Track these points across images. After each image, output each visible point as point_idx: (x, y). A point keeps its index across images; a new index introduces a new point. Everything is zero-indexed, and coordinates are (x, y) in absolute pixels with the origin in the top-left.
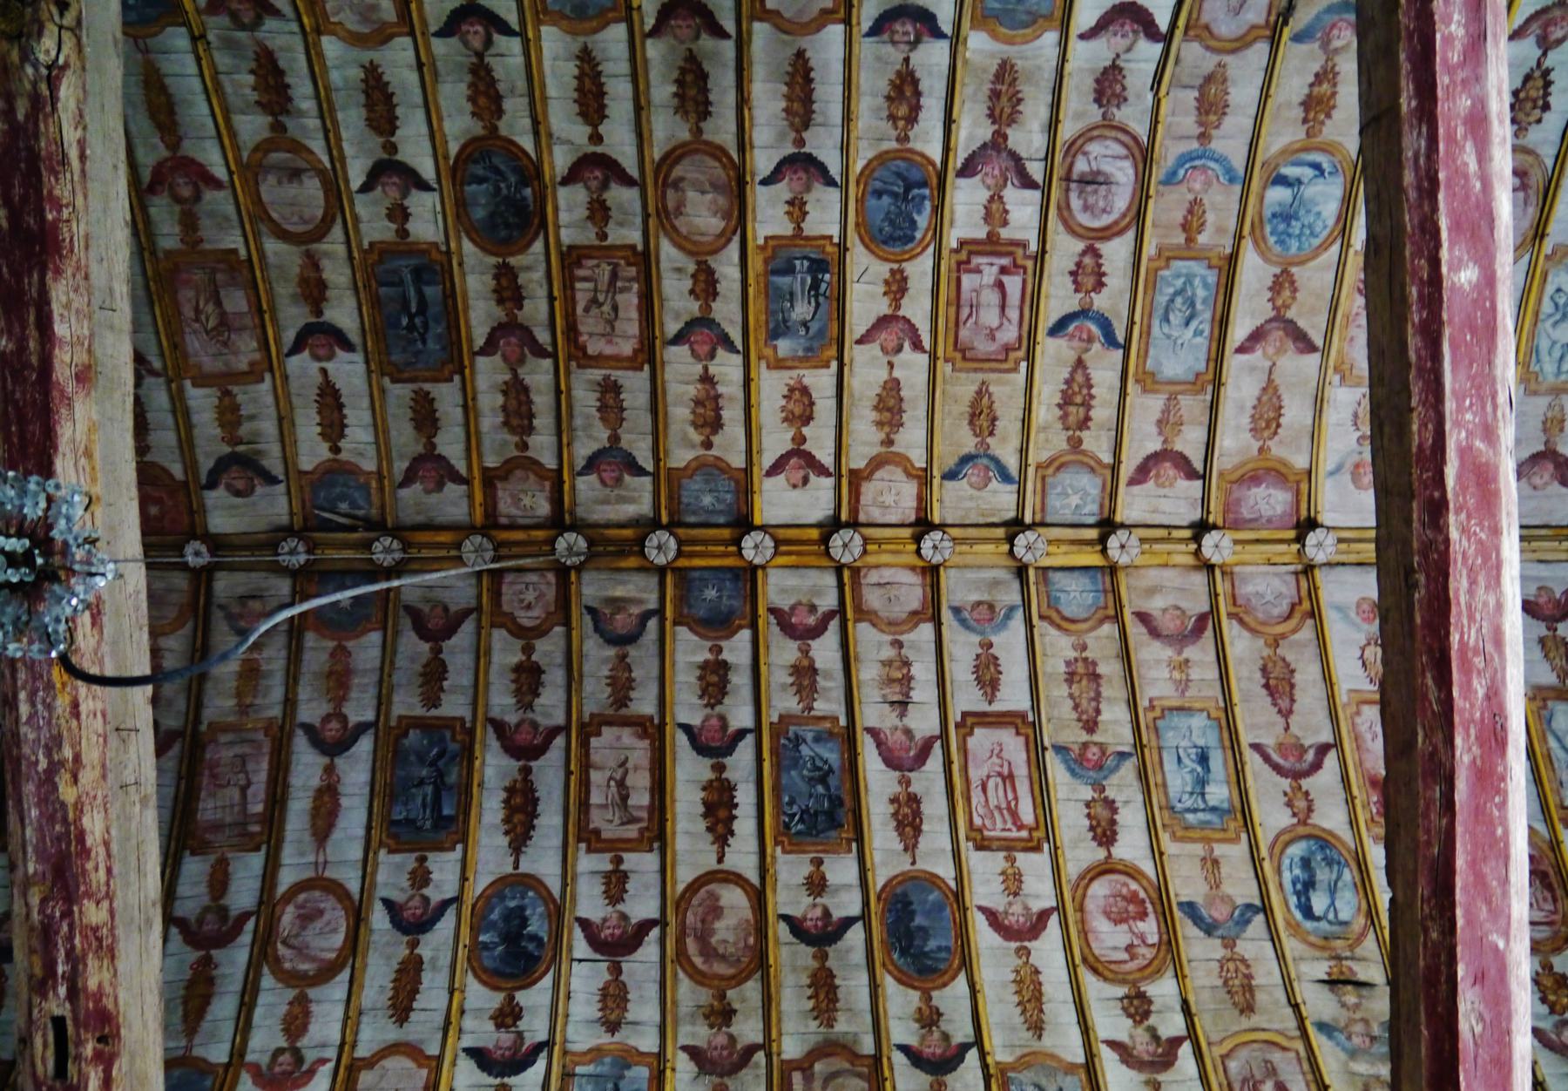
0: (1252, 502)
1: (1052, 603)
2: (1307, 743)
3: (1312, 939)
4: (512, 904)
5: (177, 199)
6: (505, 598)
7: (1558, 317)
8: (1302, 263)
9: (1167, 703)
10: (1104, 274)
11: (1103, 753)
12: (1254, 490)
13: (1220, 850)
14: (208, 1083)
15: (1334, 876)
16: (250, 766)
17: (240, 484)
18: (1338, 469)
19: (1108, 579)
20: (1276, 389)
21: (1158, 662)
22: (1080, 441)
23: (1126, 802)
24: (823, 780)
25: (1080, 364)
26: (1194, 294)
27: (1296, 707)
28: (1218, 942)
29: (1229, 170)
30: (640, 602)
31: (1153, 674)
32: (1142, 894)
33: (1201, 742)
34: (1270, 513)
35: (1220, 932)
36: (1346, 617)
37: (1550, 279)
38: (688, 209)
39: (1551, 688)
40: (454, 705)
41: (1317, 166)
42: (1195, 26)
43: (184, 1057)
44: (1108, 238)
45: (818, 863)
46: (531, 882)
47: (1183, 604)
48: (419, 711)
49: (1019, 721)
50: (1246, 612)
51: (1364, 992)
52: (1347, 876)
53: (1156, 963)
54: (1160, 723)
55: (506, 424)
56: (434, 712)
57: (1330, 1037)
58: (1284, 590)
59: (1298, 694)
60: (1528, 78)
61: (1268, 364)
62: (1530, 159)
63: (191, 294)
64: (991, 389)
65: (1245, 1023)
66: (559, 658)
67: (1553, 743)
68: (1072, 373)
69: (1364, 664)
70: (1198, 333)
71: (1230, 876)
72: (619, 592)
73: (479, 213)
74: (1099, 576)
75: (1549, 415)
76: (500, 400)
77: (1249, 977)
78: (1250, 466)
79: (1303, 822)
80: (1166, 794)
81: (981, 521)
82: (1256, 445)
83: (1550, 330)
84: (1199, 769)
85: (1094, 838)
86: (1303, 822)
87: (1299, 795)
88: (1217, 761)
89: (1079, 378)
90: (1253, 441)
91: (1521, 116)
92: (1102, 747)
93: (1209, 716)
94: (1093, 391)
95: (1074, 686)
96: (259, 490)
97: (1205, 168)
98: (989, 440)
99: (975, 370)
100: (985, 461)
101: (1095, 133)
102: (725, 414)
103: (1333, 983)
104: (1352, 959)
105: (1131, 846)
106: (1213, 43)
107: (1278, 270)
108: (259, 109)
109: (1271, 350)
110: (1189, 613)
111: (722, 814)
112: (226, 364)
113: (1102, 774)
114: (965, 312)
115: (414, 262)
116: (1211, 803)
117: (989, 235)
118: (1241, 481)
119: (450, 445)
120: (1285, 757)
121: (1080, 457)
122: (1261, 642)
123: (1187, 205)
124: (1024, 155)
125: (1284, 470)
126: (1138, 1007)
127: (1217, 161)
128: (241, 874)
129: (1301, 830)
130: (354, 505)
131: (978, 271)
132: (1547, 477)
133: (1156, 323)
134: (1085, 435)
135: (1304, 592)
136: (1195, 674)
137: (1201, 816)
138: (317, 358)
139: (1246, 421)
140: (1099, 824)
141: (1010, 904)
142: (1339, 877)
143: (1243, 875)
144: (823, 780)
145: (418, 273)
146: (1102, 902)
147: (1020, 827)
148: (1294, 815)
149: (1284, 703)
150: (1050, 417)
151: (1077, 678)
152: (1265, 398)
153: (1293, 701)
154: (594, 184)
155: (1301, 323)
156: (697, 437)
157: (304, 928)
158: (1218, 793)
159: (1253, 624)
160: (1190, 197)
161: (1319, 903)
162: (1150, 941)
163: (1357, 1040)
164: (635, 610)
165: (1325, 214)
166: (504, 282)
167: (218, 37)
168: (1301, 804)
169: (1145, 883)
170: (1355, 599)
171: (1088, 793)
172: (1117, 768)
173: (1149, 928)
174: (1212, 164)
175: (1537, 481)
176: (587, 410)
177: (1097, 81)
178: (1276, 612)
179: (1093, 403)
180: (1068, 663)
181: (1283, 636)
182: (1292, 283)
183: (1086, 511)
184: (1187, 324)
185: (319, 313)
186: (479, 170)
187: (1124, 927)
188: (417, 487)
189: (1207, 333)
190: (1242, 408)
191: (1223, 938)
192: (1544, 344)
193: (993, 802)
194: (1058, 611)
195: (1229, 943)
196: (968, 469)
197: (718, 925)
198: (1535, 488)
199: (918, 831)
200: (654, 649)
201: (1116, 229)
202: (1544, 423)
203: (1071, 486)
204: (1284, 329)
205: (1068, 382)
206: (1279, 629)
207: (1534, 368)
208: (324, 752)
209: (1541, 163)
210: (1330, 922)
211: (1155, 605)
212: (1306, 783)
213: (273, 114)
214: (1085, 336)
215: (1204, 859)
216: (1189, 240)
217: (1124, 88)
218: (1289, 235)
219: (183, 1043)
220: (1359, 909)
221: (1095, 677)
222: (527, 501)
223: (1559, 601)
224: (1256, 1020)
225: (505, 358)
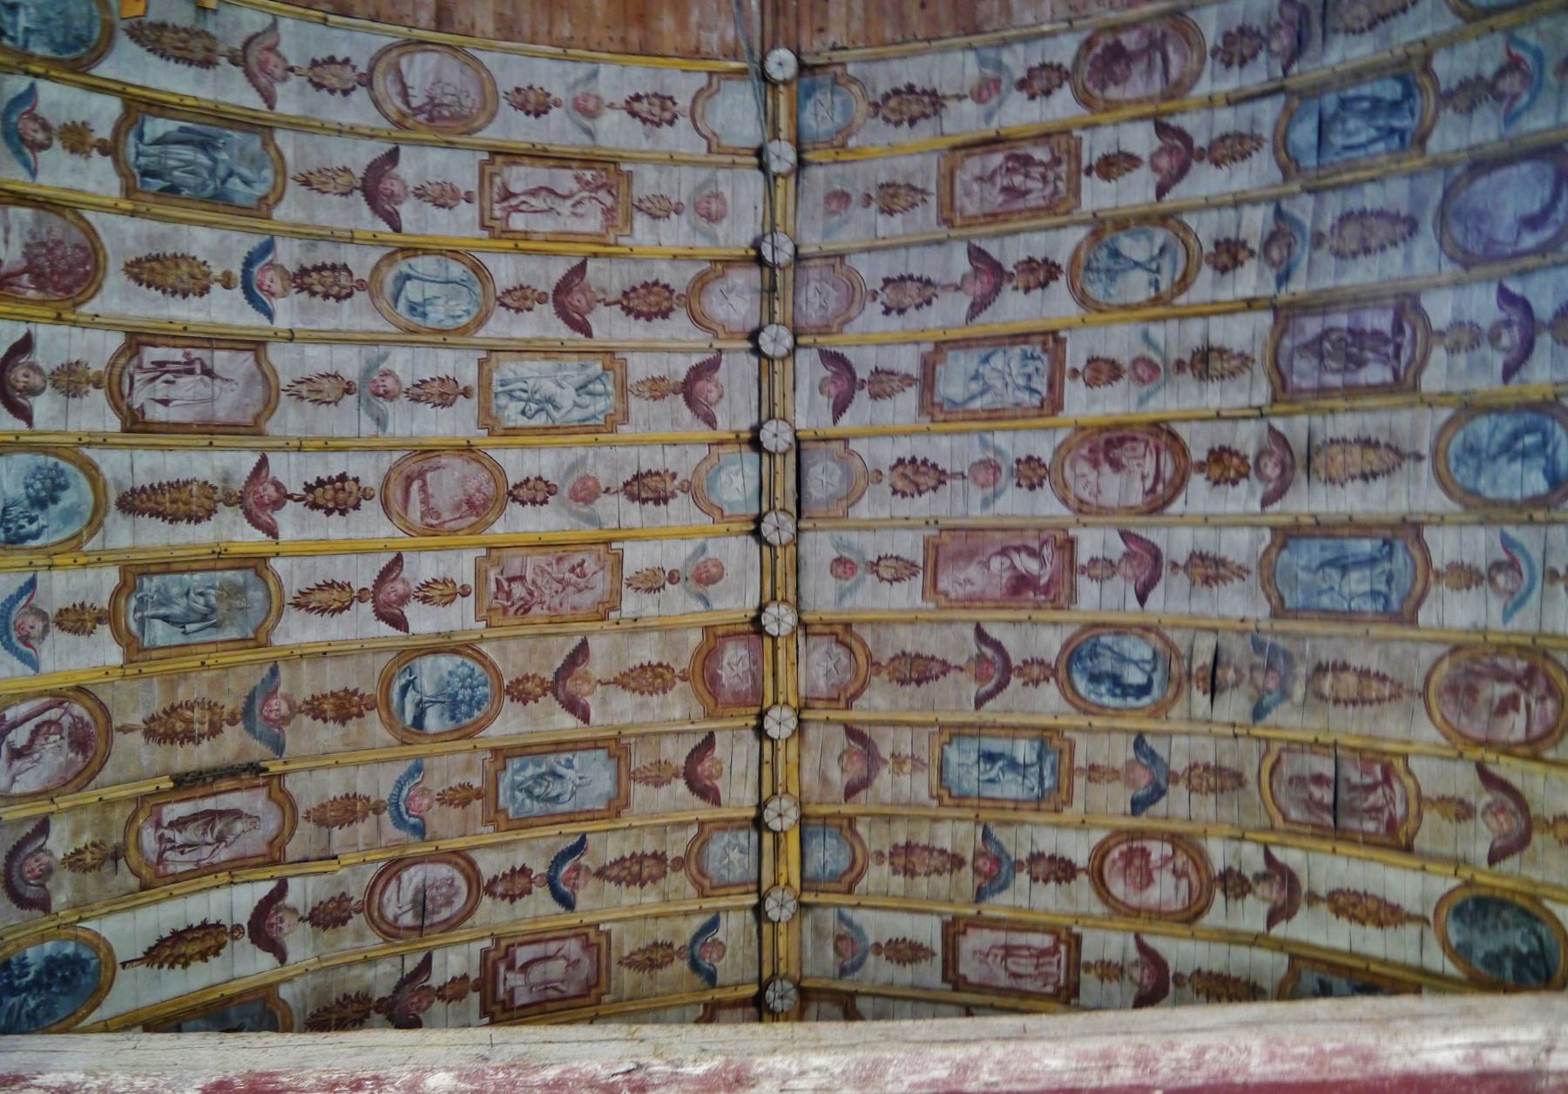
1: (836, 878)
2: (974, 650)
3: (1170, 693)
7: (550, 407)
8: (499, 676)
10: (513, 870)
15: (1108, 653)
20: (625, 675)
21: (893, 784)
25: (601, 874)
26: (532, 777)
27: (939, 656)
28: (1171, 788)
31: (906, 790)
33: (974, 756)
35: (1162, 782)
36: (850, 590)
37: (511, 424)
39: (922, 396)
41: (404, 690)
42: (271, 854)
44: (478, 873)
47: (837, 752)
49: (952, 930)
51: (1223, 658)
52: (1107, 640)
53: (1192, 853)
54: (955, 792)
57: (1268, 710)
58: (823, 649)
59: (927, 652)
60: (314, 506)
64: (626, 953)
65: (1252, 786)
68: (610, 879)
69: (898, 580)
70: (570, 765)
77: (1207, 768)
78: (700, 687)
80: (1025, 801)
81: (755, 943)
82: (679, 684)
84: (1000, 763)
85: (1068, 881)
86: (1055, 672)
87: (1027, 670)
89: (615, 872)
90: (676, 688)
91: (352, 500)
94: (627, 855)
97: (409, 799)
98: (676, 947)
99: (609, 971)
100: (697, 948)
101: (376, 914)
103: (1214, 689)
105: (1078, 849)
106: (286, 832)
109: (586, 688)
114: (552, 994)
116: (1034, 758)
117: (475, 990)
118: (714, 695)
120: (989, 678)
122: (875, 679)
124: (399, 977)
125: (704, 652)
126: (1234, 883)
127: (401, 790)
129: (1062, 674)
131: (511, 992)
132: (711, 386)
133: (560, 808)
134: (670, 855)
136: (906, 750)
137: (1047, 772)
139: (656, 699)
141: (1131, 978)
142: (1110, 648)
146: (1131, 890)
147: (1056, 950)
148: (1047, 679)
149: (936, 668)
150: (654, 893)
151: (910, 866)
152: (633, 684)
153: (933, 658)
155: (558, 663)
159: (857, 685)
160: (436, 805)
161: (1135, 677)
163: (1271, 685)
165: (450, 667)
168: (1036, 671)
170: (832, 580)
171: (1023, 878)
172: (998, 844)
174: (405, 792)
175: (713, 396)
177: (326, 928)
178: (844, 660)
179: (639, 852)
180: (895, 872)
181: (869, 656)
182: (518, 681)
183: (745, 843)
184: (561, 777)
187: (1156, 875)
189: (569, 756)
190: (642, 706)
191: (1168, 781)
192: (577, 414)
193: (1031, 970)
194: (845, 874)
195: (1173, 778)
196: (706, 963)
198: (721, 396)
201: (469, 869)
202: (655, 399)
203: (721, 861)
205: (619, 882)
206: (862, 659)
209: (398, 464)
210: (1154, 669)
211: (838, 778)
212: (1016, 661)
215: (1089, 779)
216: (479, 795)
217: (333, 899)
218: (472, 698)
221: (909, 847)
223: (835, 373)
224: (1250, 774)
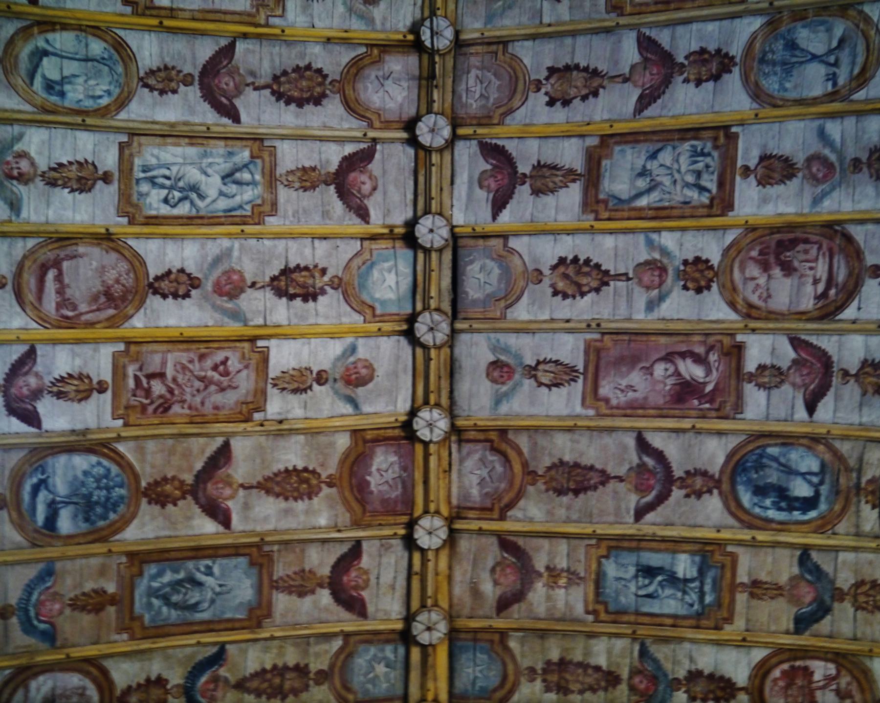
0: (385, 488)
2: (635, 460)
3: (837, 508)
7: (194, 196)
8: (136, 477)
9: (591, 596)
11: (639, 672)
12: (373, 487)
13: (743, 577)
18: (352, 401)
19: (463, 636)
20: (268, 479)
21: (549, 598)
22: (320, 672)
23: (692, 660)
27: (598, 466)
31: (561, 604)
32: (786, 666)
33: (632, 570)
34: (396, 468)
35: (827, 598)
36: (506, 395)
41: (36, 490)
47: (490, 563)
50: (500, 499)
54: (611, 608)
58: (477, 456)
59: (585, 461)
61: (241, 492)
62: (28, 264)
67: (643, 202)
68: (249, 691)
69: (557, 385)
70: (209, 572)
71: (770, 573)
74: (459, 644)
75: (297, 185)
78: (347, 494)
79: (718, 483)
80: (685, 617)
82: (326, 490)
83: (208, 200)
84: (660, 578)
87: (689, 481)
89: (255, 684)
90: (321, 495)
92: (634, 672)
93: (607, 557)
94: (268, 667)
95: (572, 687)
97: (40, 603)
104: (860, 471)
107: (144, 501)
109: (228, 492)
110: (499, 559)
113: (662, 678)
116: (695, 574)
120: (650, 488)
121: (337, 670)
122: (531, 489)
123: (77, 614)
125: (352, 458)
129: (725, 486)
132: (364, 178)
133: (199, 616)
134: (314, 667)
135: (481, 436)
137: (707, 588)
139: (301, 506)
140: (712, 692)
142: (775, 459)
143: (770, 559)
148: (710, 491)
149: (595, 479)
151: (563, 683)
152: (277, 489)
153: (592, 468)
155: (199, 465)
160: (68, 611)
161: (801, 489)
162: (833, 672)
168: (699, 482)
169: (774, 661)
170: (488, 383)
172: (656, 661)
174: (34, 597)
175: (366, 188)
176: (293, 56)
178: (499, 469)
181: (525, 465)
182: (157, 483)
189: (209, 562)
190: (287, 512)
192: (223, 204)
194: (495, 690)
195: (839, 595)
198: (375, 189)
201: (101, 678)
202: (305, 189)
204: (205, 483)
205: (258, 694)
206: (517, 468)
207: (248, 210)
209: (32, 252)
210: (821, 483)
212: (678, 473)
214: (212, 686)
215: (752, 595)
218: (108, 499)
220: (809, 448)
221: (563, 664)
223: (495, 167)
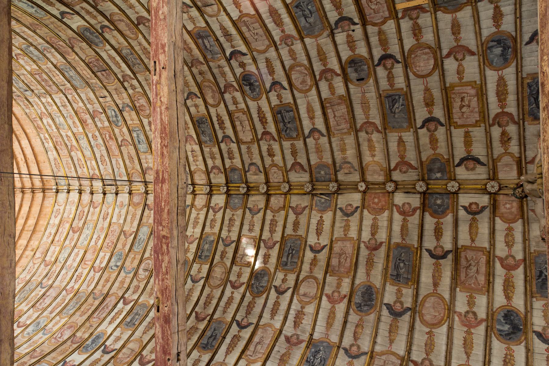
4: (255, 93)
5: (339, 292)
6: (281, 175)
14: (305, 33)
16: (335, 123)
17: (349, 208)
24: (203, 131)
29: (124, 269)
30: (250, 174)
38: (221, 273)
40: (287, 144)
41: (112, 269)
43: (317, 38)
45: (198, 112)
46: (254, 99)
48: (295, 142)
55: (277, 222)
56: (292, 142)
63: (346, 265)
66: (265, 159)
72: (255, 177)
73: (266, 278)
76: (277, 229)
88: (137, 142)
96: (344, 206)
102: (228, 222)
108: (305, 313)
111: (220, 121)
112: (343, 243)
115: (286, 267)
119: (292, 217)
128: (326, 91)
130: (320, 201)
138: (319, 243)
144: (203, 131)
145: (286, 265)
154: (238, 282)
156: (235, 217)
157: (303, 79)
158: (135, 135)
164: (251, 172)
166: (267, 260)
167: (306, 334)
173: (137, 105)
185: (315, 256)
186: (261, 289)
188: (303, 206)
197: (211, 94)
199: (308, 108)
200: (245, 162)
208: (316, 129)
213: (302, 311)
219: (319, 41)
222: (276, 201)
225: (273, 240)
